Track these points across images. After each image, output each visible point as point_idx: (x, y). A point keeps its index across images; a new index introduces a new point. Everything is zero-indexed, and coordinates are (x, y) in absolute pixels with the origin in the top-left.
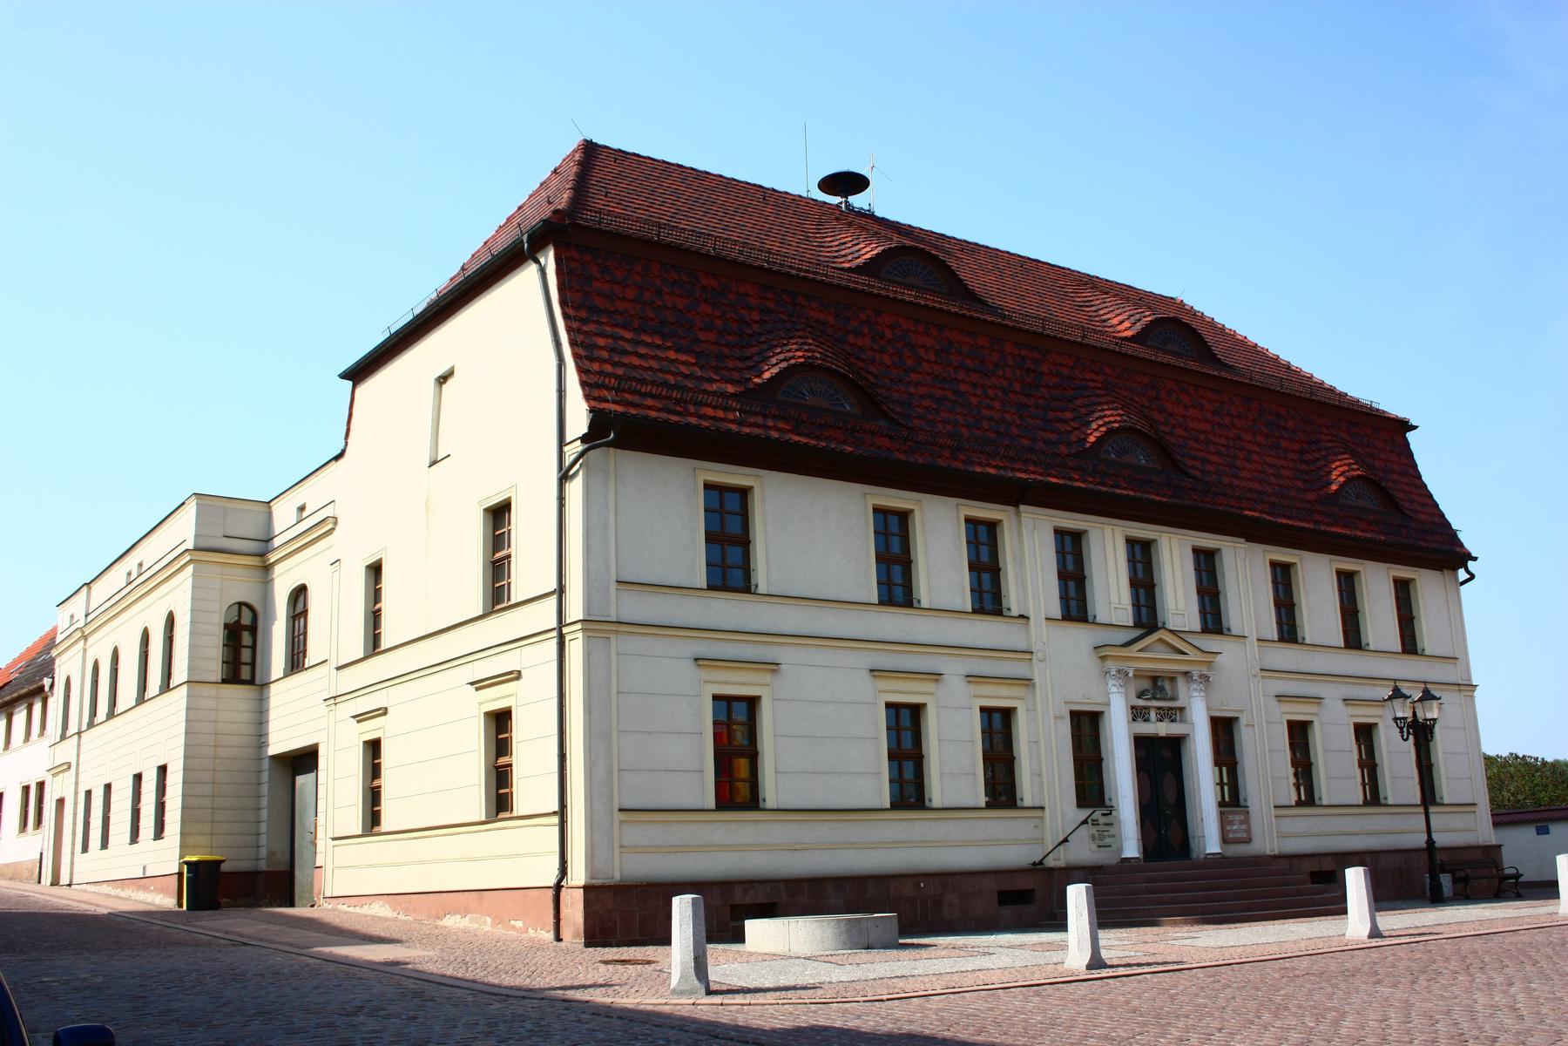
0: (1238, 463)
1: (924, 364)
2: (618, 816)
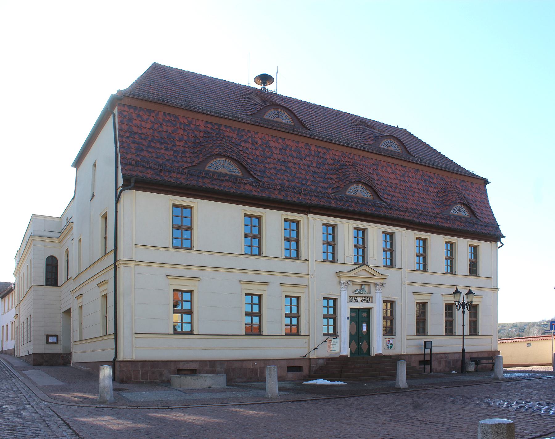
0: (408, 197)
1: (274, 155)
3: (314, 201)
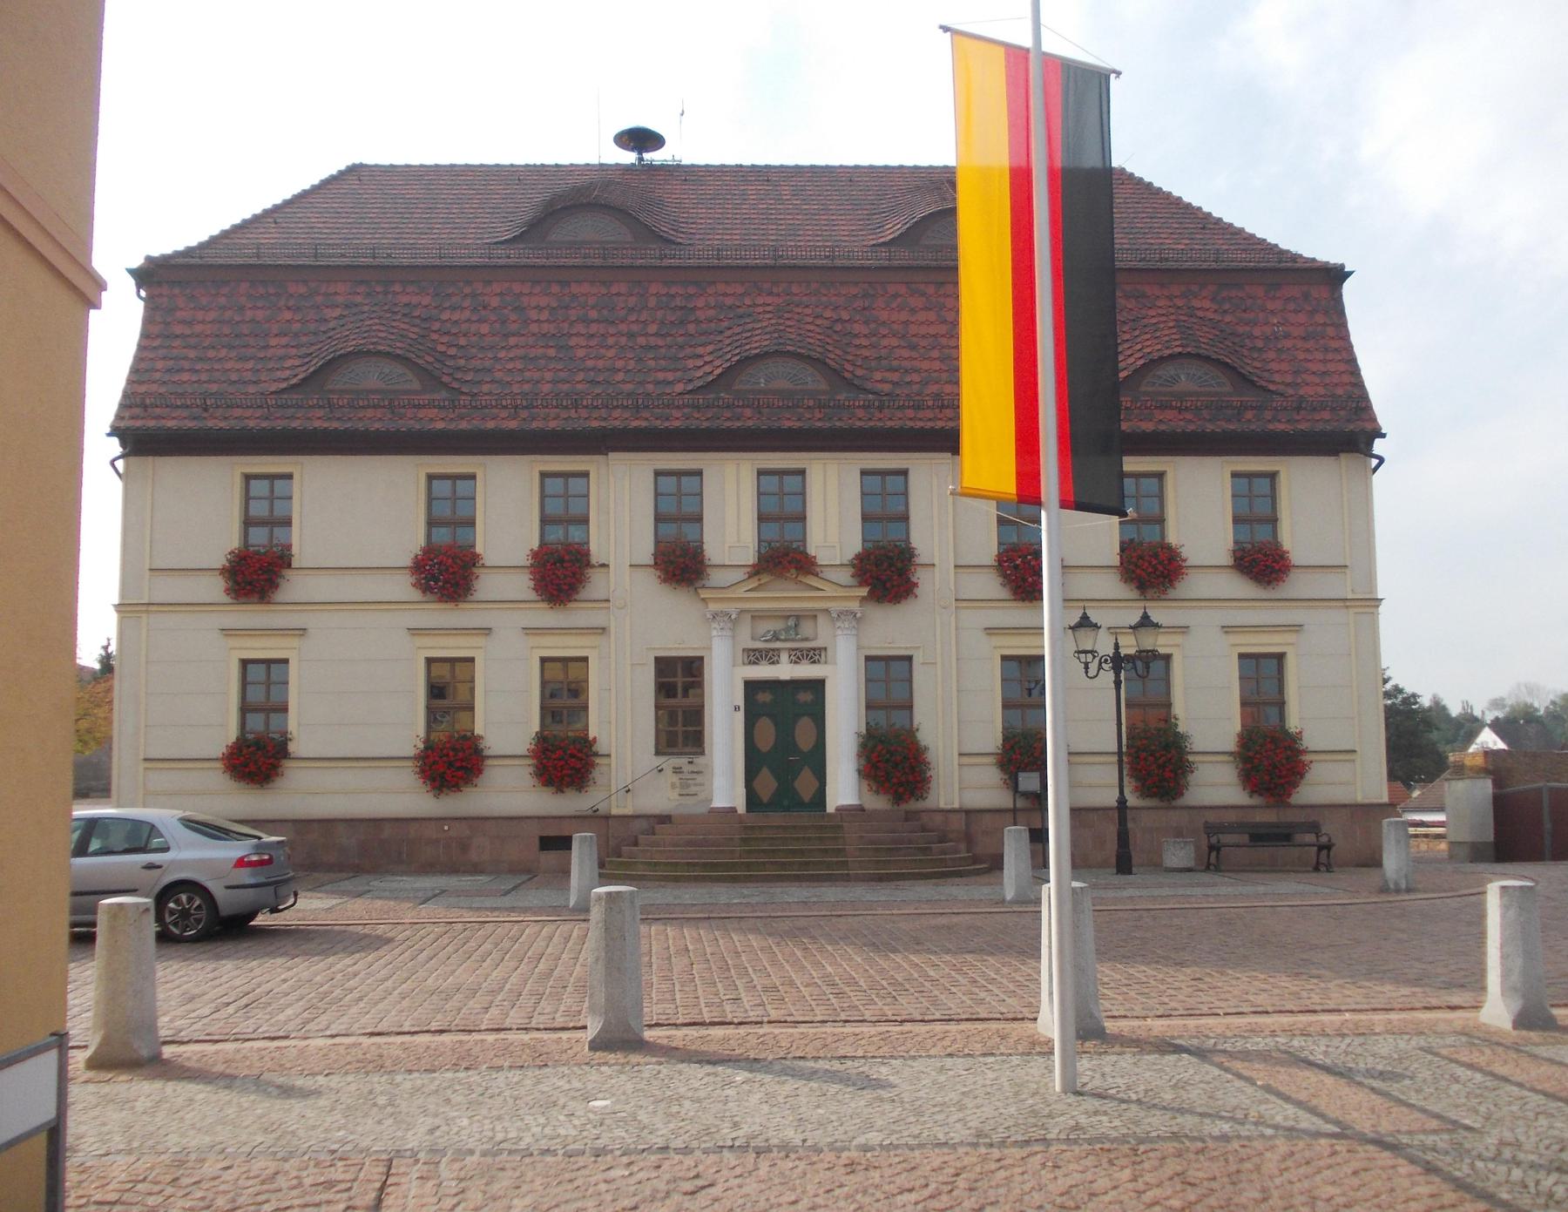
2: (143, 765)
3: (619, 419)
